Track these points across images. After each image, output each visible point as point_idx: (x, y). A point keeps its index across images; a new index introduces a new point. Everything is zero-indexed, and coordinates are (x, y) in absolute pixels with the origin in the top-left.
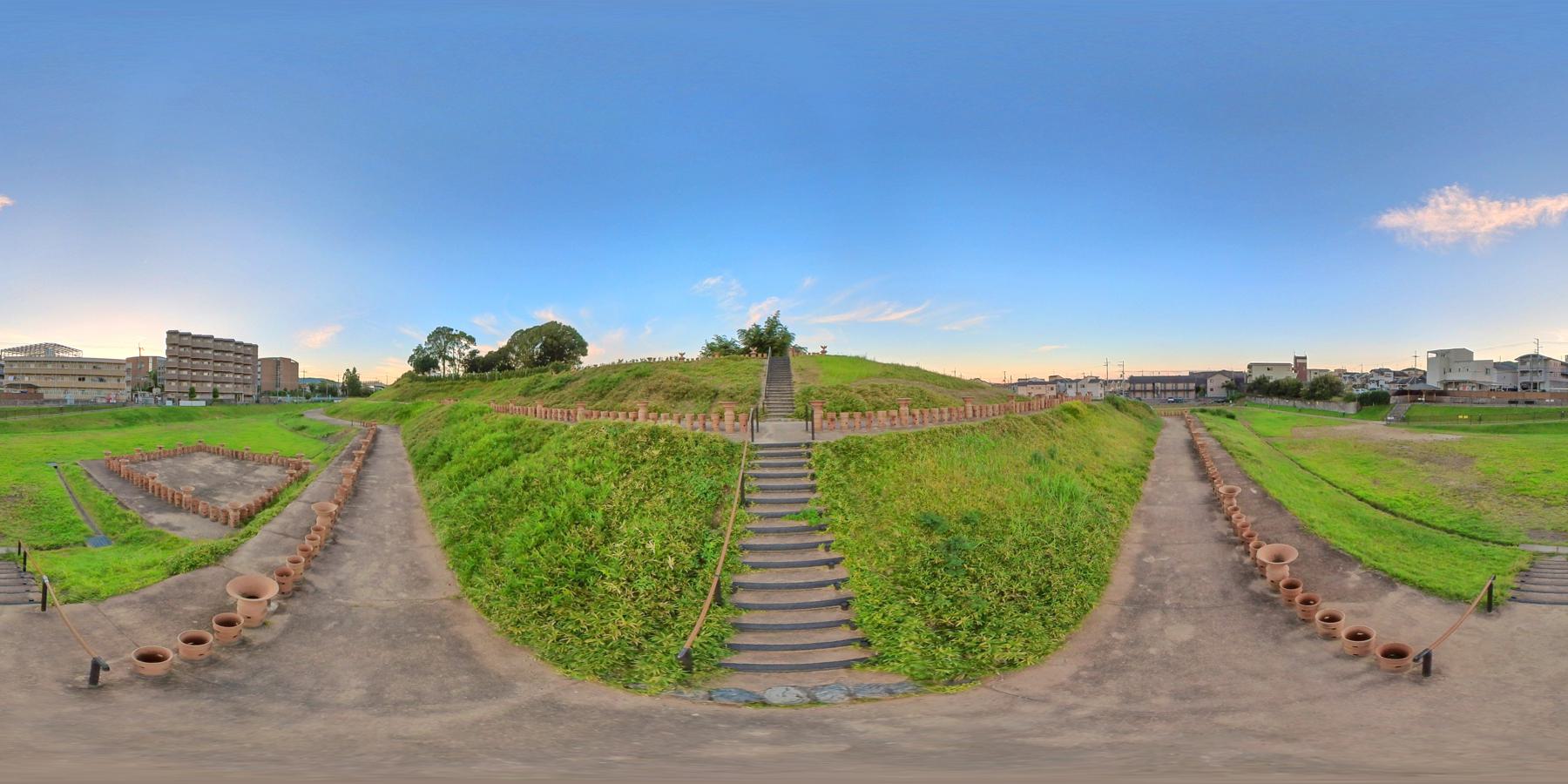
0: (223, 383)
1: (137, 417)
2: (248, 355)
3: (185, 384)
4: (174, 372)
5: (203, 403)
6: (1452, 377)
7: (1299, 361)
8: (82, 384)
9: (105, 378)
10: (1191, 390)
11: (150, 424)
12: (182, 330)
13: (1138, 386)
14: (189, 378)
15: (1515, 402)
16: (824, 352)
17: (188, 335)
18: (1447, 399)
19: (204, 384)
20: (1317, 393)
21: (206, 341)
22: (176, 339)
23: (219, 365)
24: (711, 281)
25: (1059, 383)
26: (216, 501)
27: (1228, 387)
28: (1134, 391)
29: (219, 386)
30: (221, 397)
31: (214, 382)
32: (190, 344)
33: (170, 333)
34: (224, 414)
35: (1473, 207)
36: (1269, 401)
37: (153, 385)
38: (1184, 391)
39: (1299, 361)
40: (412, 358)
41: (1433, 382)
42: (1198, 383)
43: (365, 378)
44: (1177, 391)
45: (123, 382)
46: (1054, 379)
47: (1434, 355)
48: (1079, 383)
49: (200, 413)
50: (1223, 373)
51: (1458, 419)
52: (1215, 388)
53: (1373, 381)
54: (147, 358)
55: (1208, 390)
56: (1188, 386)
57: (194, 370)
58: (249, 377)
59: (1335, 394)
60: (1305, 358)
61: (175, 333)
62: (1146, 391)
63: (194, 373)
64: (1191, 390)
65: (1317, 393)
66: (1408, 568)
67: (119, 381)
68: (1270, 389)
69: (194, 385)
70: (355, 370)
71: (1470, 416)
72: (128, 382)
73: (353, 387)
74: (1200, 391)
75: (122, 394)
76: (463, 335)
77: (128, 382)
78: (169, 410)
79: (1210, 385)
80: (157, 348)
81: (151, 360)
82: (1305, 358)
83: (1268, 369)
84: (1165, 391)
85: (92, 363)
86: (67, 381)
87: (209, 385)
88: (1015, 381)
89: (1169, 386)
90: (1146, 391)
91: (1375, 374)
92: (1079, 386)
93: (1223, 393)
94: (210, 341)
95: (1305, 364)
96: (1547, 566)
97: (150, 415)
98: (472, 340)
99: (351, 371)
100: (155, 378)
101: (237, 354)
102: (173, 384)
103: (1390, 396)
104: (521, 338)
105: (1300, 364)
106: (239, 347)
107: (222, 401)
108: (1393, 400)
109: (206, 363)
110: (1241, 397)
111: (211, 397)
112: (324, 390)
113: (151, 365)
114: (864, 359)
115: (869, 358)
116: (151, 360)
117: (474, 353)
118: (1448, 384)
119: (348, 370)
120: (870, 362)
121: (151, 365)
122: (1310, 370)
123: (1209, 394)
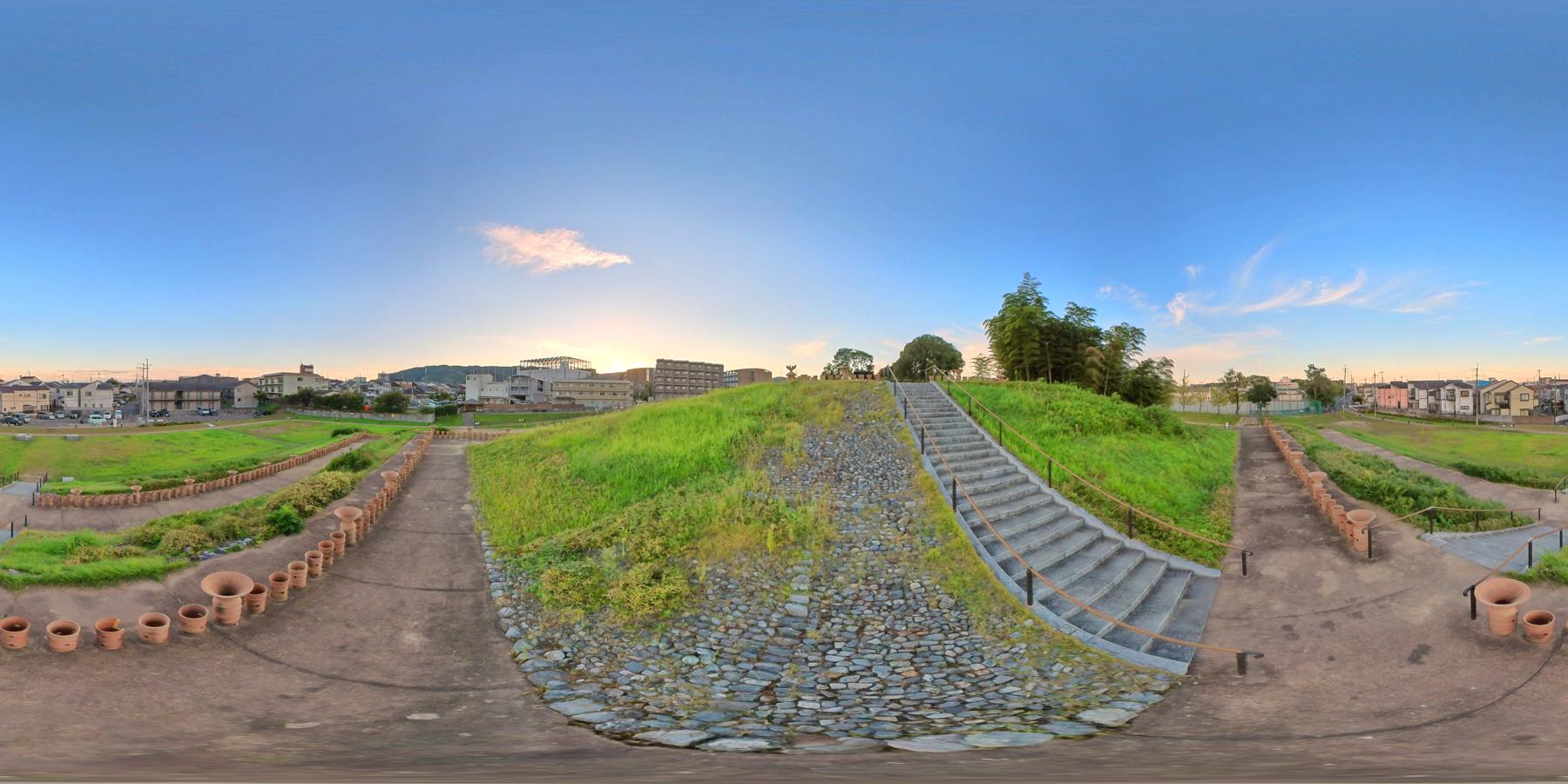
4: (661, 387)
6: (486, 394)
8: (602, 397)
12: (706, 362)
15: (537, 411)
17: (671, 361)
33: (659, 361)
36: (325, 413)
45: (628, 395)
48: (83, 390)
52: (243, 397)
53: (372, 391)
54: (645, 369)
55: (236, 400)
72: (631, 395)
74: (227, 399)
77: (631, 395)
79: (237, 394)
80: (653, 365)
81: (648, 372)
83: (299, 379)
91: (375, 385)
92: (83, 394)
94: (687, 365)
96: (963, 465)
105: (306, 370)
113: (648, 376)
116: (648, 372)
121: (648, 376)
123: (237, 404)
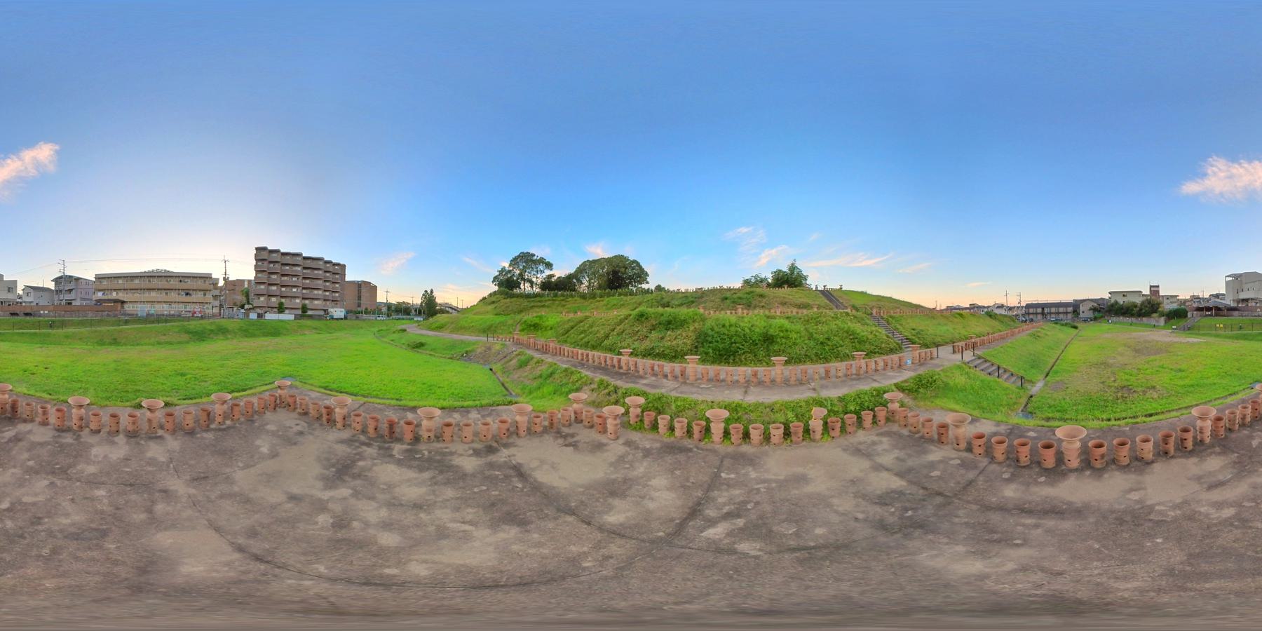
0: (313, 299)
1: (212, 331)
2: (337, 274)
3: (274, 299)
4: (262, 287)
5: (292, 317)
6: (1243, 296)
7: (1153, 289)
9: (191, 292)
10: (1069, 313)
11: (227, 339)
13: (1031, 310)
14: (331, 299)
16: (841, 288)
18: (1236, 313)
19: (293, 300)
20: (1144, 311)
21: (295, 258)
22: (264, 255)
23: (308, 281)
24: (744, 230)
25: (976, 309)
26: (900, 474)
27: (1094, 310)
28: (1029, 314)
29: (307, 302)
30: (310, 313)
31: (303, 298)
32: (279, 260)
33: (258, 249)
34: (316, 329)
35: (1241, 170)
37: (245, 301)
38: (1064, 313)
39: (1153, 289)
40: (495, 278)
41: (1229, 302)
42: (1075, 306)
43: (440, 299)
44: (1059, 313)
46: (972, 306)
47: (1231, 279)
49: (288, 326)
50: (1092, 300)
51: (1216, 327)
55: (1081, 312)
56: (1058, 310)
57: (283, 286)
58: (337, 295)
59: (1155, 312)
60: (1158, 287)
61: (264, 249)
62: (1037, 314)
63: (283, 289)
64: (1069, 313)
65: (1144, 311)
66: (182, 406)
67: (205, 295)
68: (1117, 310)
69: (283, 300)
70: (432, 291)
71: (1224, 325)
73: (430, 308)
75: (208, 308)
76: (542, 261)
78: (252, 323)
79: (1082, 309)
82: (1158, 287)
84: (1051, 313)
85: (179, 277)
86: (173, 296)
87: (298, 301)
88: (944, 307)
89: (1053, 310)
90: (1037, 314)
93: (1090, 314)
94: (321, 263)
95: (1158, 291)
97: (230, 329)
98: (549, 265)
99: (429, 292)
100: (247, 295)
101: (326, 272)
102: (262, 299)
103: (1187, 312)
104: (588, 267)
105: (1154, 290)
106: (328, 265)
107: (311, 317)
108: (1189, 315)
109: (295, 279)
110: (1102, 317)
111: (299, 312)
112: (402, 310)
114: (866, 293)
115: (868, 292)
117: (550, 276)
118: (1239, 301)
119: (426, 291)
120: (869, 295)
122: (1163, 296)
123: (1082, 315)
